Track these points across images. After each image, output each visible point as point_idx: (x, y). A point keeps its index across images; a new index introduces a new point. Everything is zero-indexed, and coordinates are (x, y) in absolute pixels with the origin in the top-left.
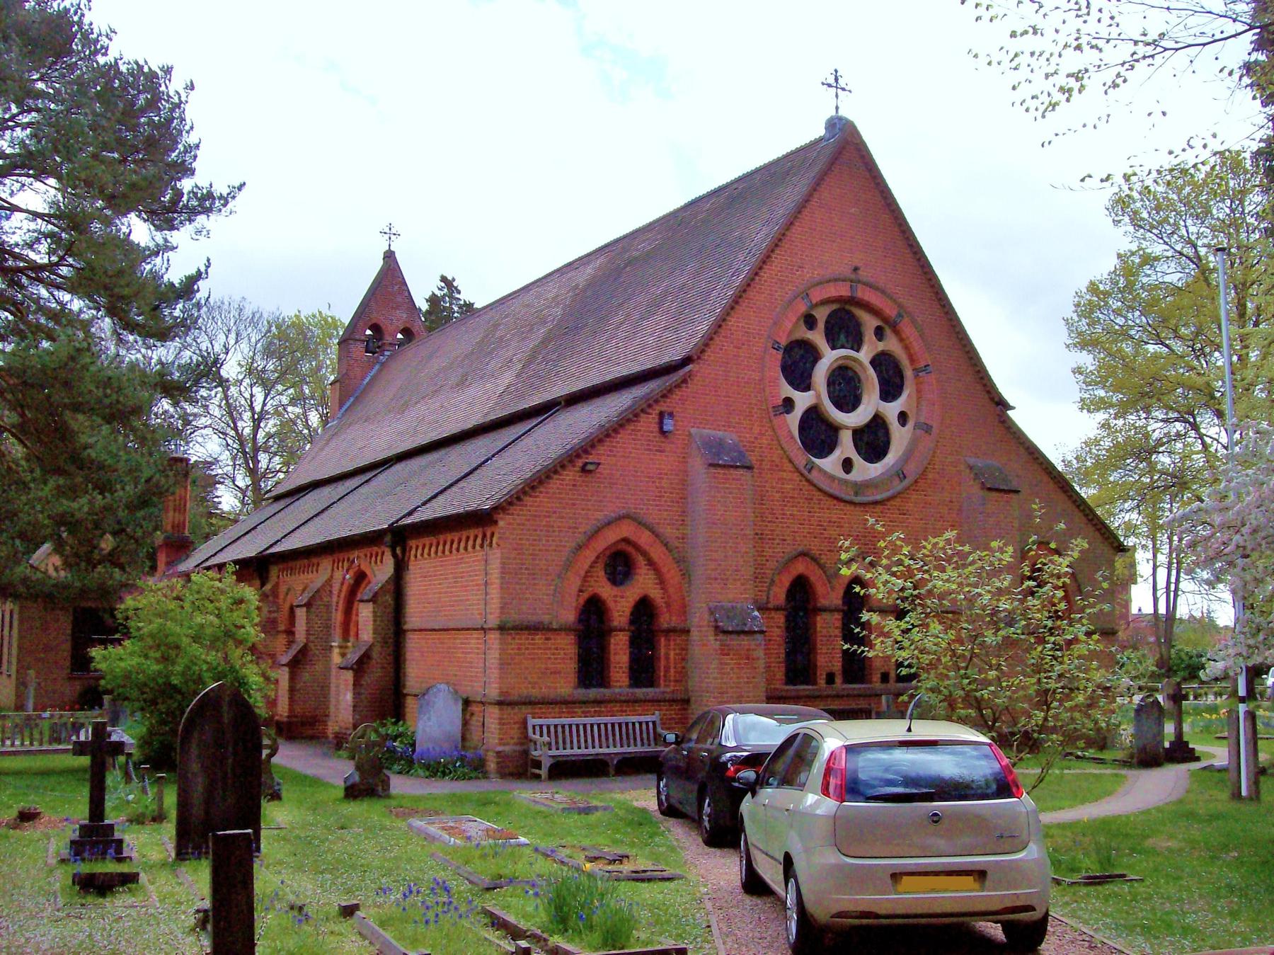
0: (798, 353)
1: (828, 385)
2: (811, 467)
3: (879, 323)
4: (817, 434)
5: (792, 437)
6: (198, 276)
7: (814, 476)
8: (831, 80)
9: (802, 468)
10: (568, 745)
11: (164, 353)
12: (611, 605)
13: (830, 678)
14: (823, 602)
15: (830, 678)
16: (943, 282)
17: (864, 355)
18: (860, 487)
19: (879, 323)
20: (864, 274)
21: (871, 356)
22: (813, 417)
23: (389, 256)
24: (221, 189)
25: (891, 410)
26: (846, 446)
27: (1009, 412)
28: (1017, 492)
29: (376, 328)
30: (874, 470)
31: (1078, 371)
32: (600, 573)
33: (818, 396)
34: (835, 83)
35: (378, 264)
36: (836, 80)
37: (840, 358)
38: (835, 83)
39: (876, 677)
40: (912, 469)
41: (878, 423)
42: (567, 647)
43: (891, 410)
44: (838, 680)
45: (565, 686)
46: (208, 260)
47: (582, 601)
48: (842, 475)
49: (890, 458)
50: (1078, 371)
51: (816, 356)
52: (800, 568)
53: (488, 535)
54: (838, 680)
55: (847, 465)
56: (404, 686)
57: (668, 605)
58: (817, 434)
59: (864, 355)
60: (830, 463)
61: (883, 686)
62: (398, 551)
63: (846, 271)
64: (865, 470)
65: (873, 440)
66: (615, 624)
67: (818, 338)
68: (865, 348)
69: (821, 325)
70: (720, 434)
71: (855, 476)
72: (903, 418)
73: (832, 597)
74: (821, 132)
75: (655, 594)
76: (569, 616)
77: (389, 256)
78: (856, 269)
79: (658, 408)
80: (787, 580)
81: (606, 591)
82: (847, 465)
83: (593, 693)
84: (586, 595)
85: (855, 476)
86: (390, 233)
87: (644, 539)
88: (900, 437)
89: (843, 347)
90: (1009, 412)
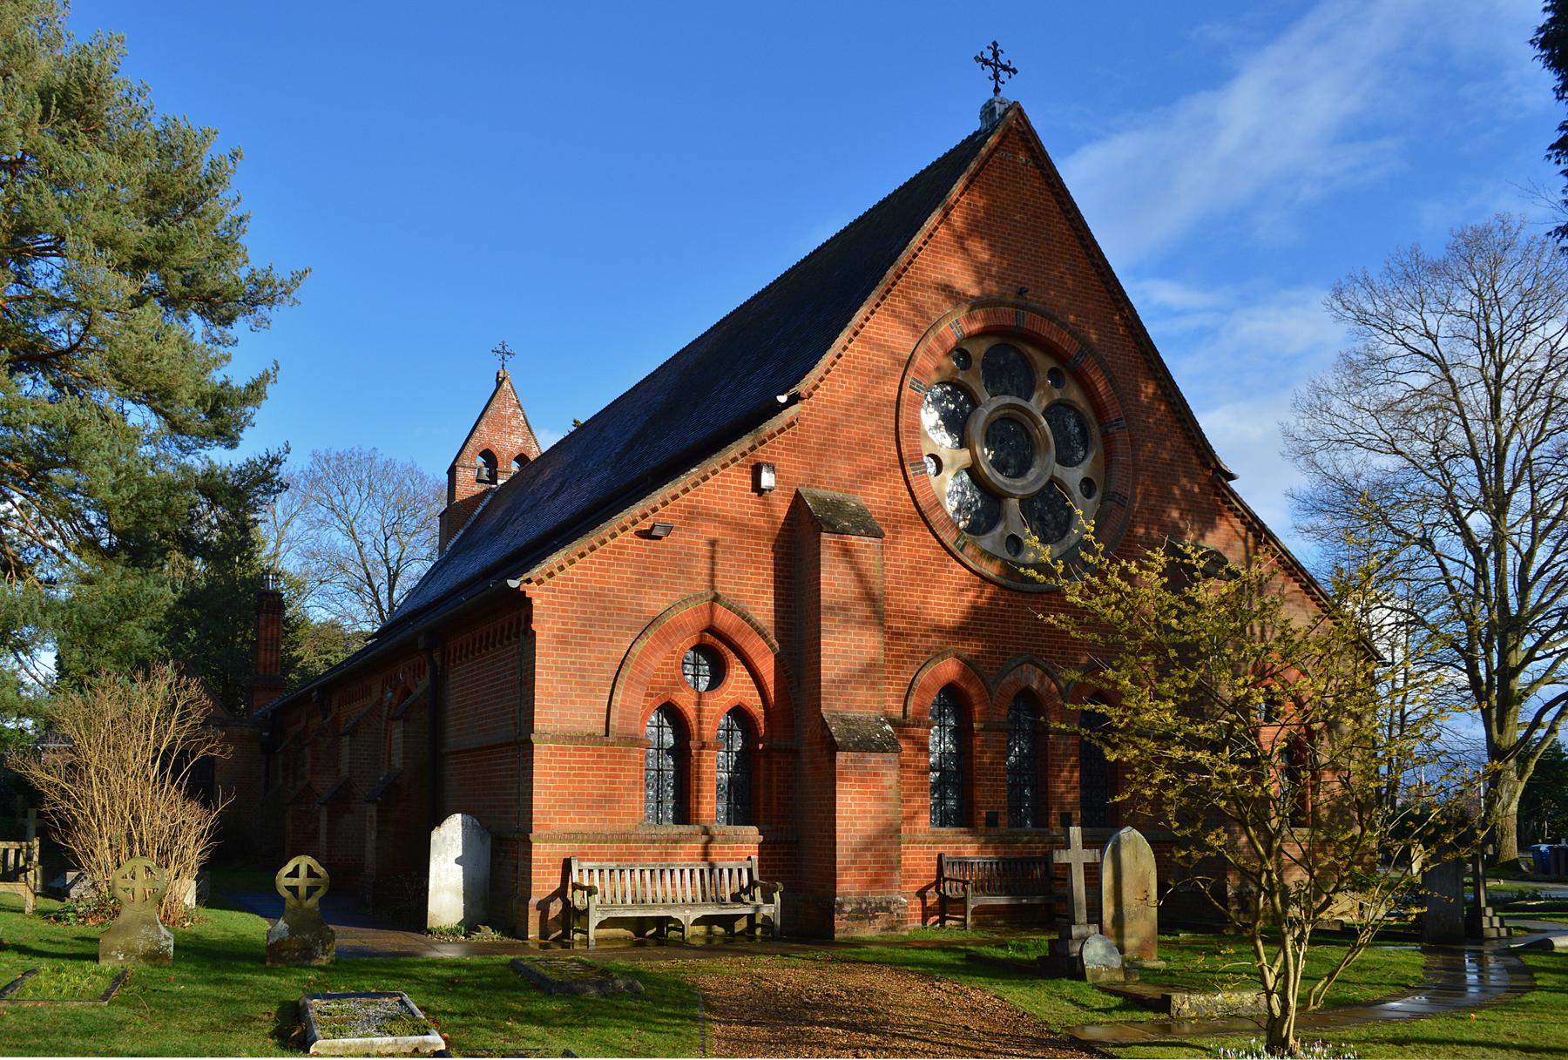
3: (1053, 365)
6: (265, 377)
8: (989, 55)
11: (221, 457)
16: (537, 778)
17: (1037, 405)
19: (1053, 365)
24: (282, 274)
25: (1073, 476)
31: (1288, 435)
34: (996, 64)
36: (996, 55)
38: (996, 64)
46: (276, 362)
50: (1288, 435)
53: (568, 1019)
56: (254, 944)
59: (1037, 405)
62: (436, 657)
69: (976, 364)
72: (1088, 486)
74: (974, 124)
75: (754, 703)
78: (1022, 292)
89: (1005, 393)
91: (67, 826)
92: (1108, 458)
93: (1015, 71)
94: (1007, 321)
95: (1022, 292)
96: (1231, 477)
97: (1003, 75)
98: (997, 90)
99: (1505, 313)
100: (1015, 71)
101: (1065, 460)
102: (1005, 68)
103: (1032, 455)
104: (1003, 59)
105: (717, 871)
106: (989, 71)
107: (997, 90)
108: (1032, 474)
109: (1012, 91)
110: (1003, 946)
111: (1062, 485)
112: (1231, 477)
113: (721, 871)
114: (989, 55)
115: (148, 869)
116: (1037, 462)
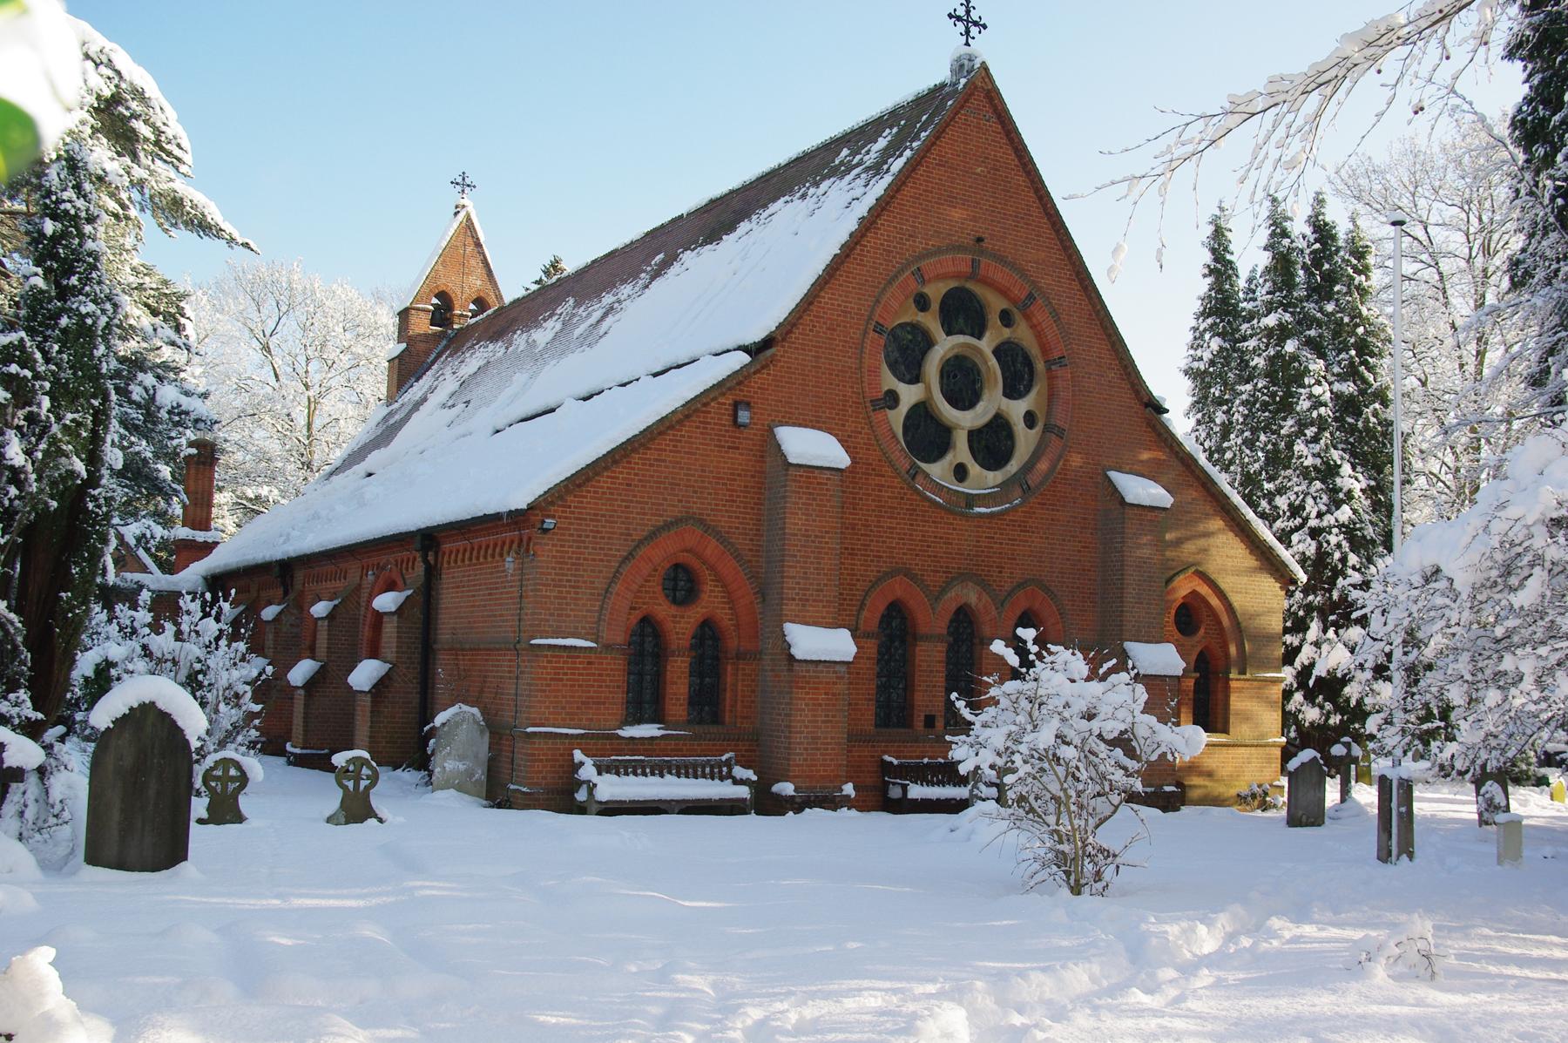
17: (986, 345)
21: (994, 345)
33: (928, 389)
34: (968, 21)
36: (968, 12)
38: (968, 21)
41: (1000, 424)
43: (1016, 410)
49: (1013, 466)
52: (897, 588)
55: (960, 472)
57: (737, 626)
59: (986, 345)
60: (939, 471)
64: (984, 480)
69: (935, 306)
81: (663, 610)
87: (712, 549)
89: (962, 332)
93: (985, 27)
96: (555, 265)
97: (974, 30)
99: (1171, 138)
100: (950, 16)
102: (976, 24)
103: (981, 388)
106: (961, 27)
108: (980, 407)
109: (984, 48)
110: (1401, 1002)
111: (910, 382)
112: (555, 265)
115: (985, 726)
116: (986, 396)
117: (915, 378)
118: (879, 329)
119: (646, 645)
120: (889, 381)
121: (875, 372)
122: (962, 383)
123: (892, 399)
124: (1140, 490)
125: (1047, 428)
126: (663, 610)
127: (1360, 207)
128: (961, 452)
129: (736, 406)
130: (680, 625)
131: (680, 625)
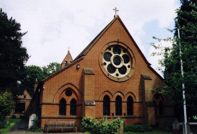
0: (107, 55)
1: (113, 60)
2: (109, 75)
4: (112, 69)
5: (106, 71)
7: (109, 77)
8: (115, 9)
9: (107, 75)
10: (66, 126)
12: (66, 100)
13: (113, 114)
14: (111, 100)
15: (125, 114)
17: (121, 55)
18: (118, 79)
20: (120, 41)
21: (122, 55)
22: (111, 65)
23: (69, 51)
25: (126, 65)
26: (117, 71)
27: (151, 66)
28: (151, 80)
29: (66, 62)
30: (123, 76)
32: (64, 93)
33: (111, 62)
34: (116, 10)
35: (67, 53)
36: (116, 9)
37: (115, 56)
39: (123, 114)
40: (130, 76)
41: (124, 67)
42: (57, 107)
43: (126, 65)
44: (115, 115)
45: (57, 115)
47: (60, 99)
48: (116, 77)
49: (126, 74)
51: (111, 55)
52: (107, 93)
54: (115, 115)
55: (117, 75)
57: (78, 100)
58: (112, 69)
60: (114, 75)
61: (124, 116)
63: (117, 40)
64: (121, 76)
65: (123, 70)
66: (67, 103)
67: (111, 52)
68: (121, 54)
70: (89, 69)
71: (119, 77)
73: (125, 99)
75: (76, 98)
76: (57, 102)
77: (69, 51)
79: (76, 64)
80: (103, 96)
81: (66, 97)
82: (117, 75)
83: (63, 116)
84: (61, 98)
85: (119, 77)
86: (69, 48)
87: (73, 88)
88: (129, 70)
89: (117, 54)
90: (151, 66)
91: (149, 78)
92: (132, 63)
94: (107, 47)
95: (118, 40)
96: (151, 65)
98: (116, 13)
101: (126, 62)
104: (117, 9)
105: (124, 110)
107: (116, 13)
109: (118, 14)
112: (151, 65)
113: (119, 112)
114: (115, 9)
116: (121, 63)
117: (109, 60)
118: (102, 53)
119: (63, 103)
120: (104, 61)
121: (101, 60)
122: (117, 60)
123: (105, 64)
124: (149, 96)
125: (132, 68)
126: (66, 97)
127: (129, 78)
128: (117, 71)
129: (77, 65)
130: (69, 100)
131: (69, 100)
